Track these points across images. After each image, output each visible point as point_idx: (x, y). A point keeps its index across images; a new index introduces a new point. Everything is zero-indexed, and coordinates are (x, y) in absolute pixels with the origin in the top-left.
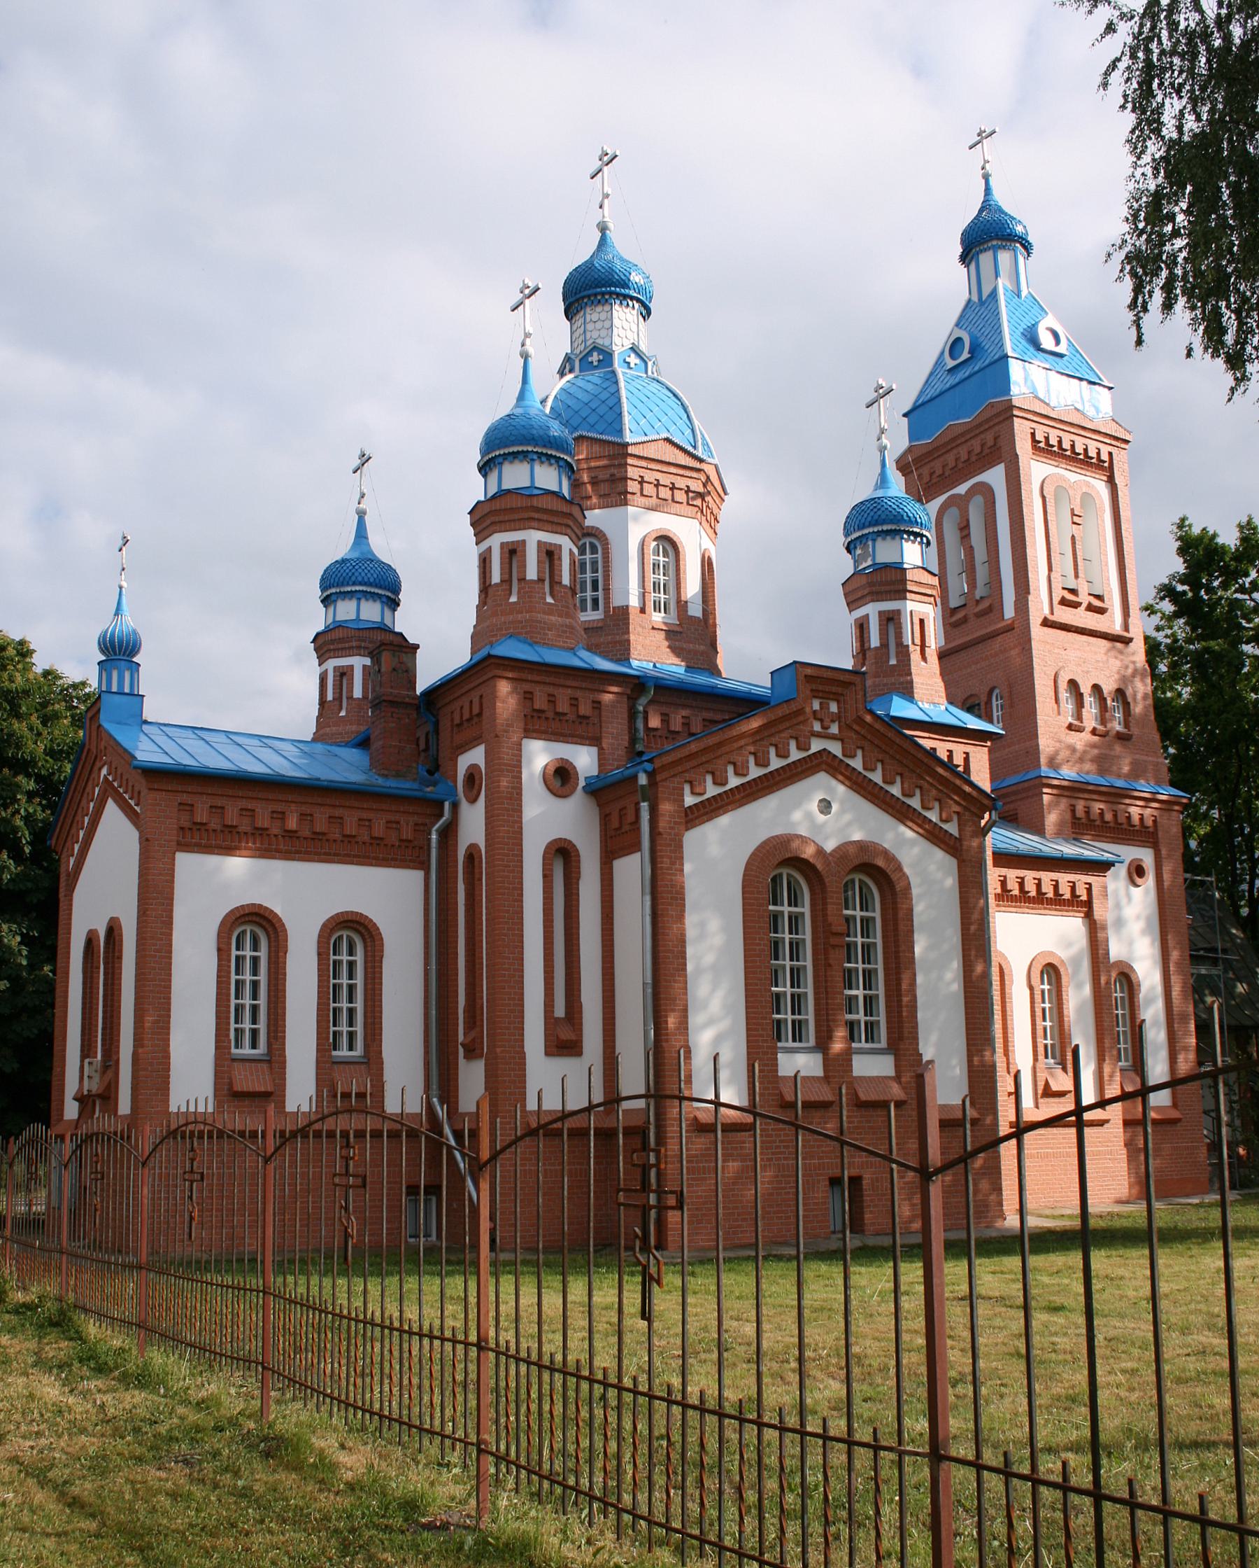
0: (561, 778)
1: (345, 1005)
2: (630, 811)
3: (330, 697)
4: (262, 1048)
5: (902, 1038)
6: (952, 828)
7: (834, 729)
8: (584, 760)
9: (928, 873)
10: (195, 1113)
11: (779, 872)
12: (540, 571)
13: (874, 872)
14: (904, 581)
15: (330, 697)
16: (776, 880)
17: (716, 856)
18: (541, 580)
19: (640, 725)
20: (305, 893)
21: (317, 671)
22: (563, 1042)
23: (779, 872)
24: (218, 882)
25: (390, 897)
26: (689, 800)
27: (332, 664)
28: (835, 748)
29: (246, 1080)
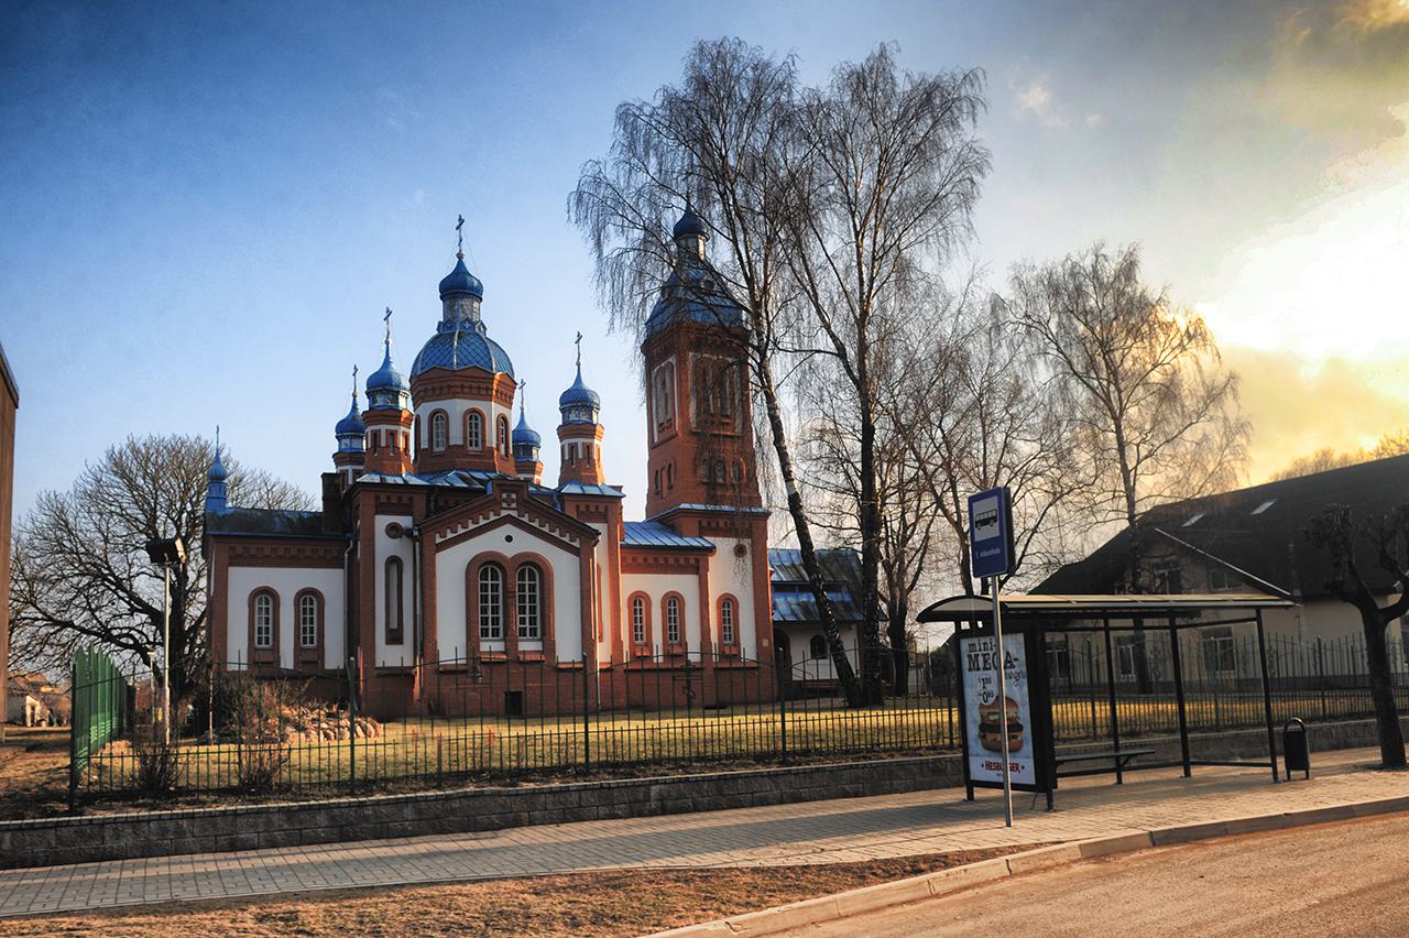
0: (393, 530)
1: (639, 616)
2: (424, 544)
3: (567, 458)
4: (645, 640)
5: (546, 636)
6: (576, 544)
7: (514, 505)
8: (405, 521)
9: (562, 566)
10: (1189, 682)
11: (485, 568)
12: (387, 442)
13: (533, 568)
14: (595, 431)
15: (567, 458)
16: (523, 571)
17: (451, 566)
18: (387, 446)
19: (432, 505)
20: (288, 581)
21: (559, 445)
22: (394, 637)
23: (485, 568)
24: (244, 580)
25: (329, 582)
26: (439, 540)
27: (567, 442)
28: (514, 514)
29: (677, 650)
